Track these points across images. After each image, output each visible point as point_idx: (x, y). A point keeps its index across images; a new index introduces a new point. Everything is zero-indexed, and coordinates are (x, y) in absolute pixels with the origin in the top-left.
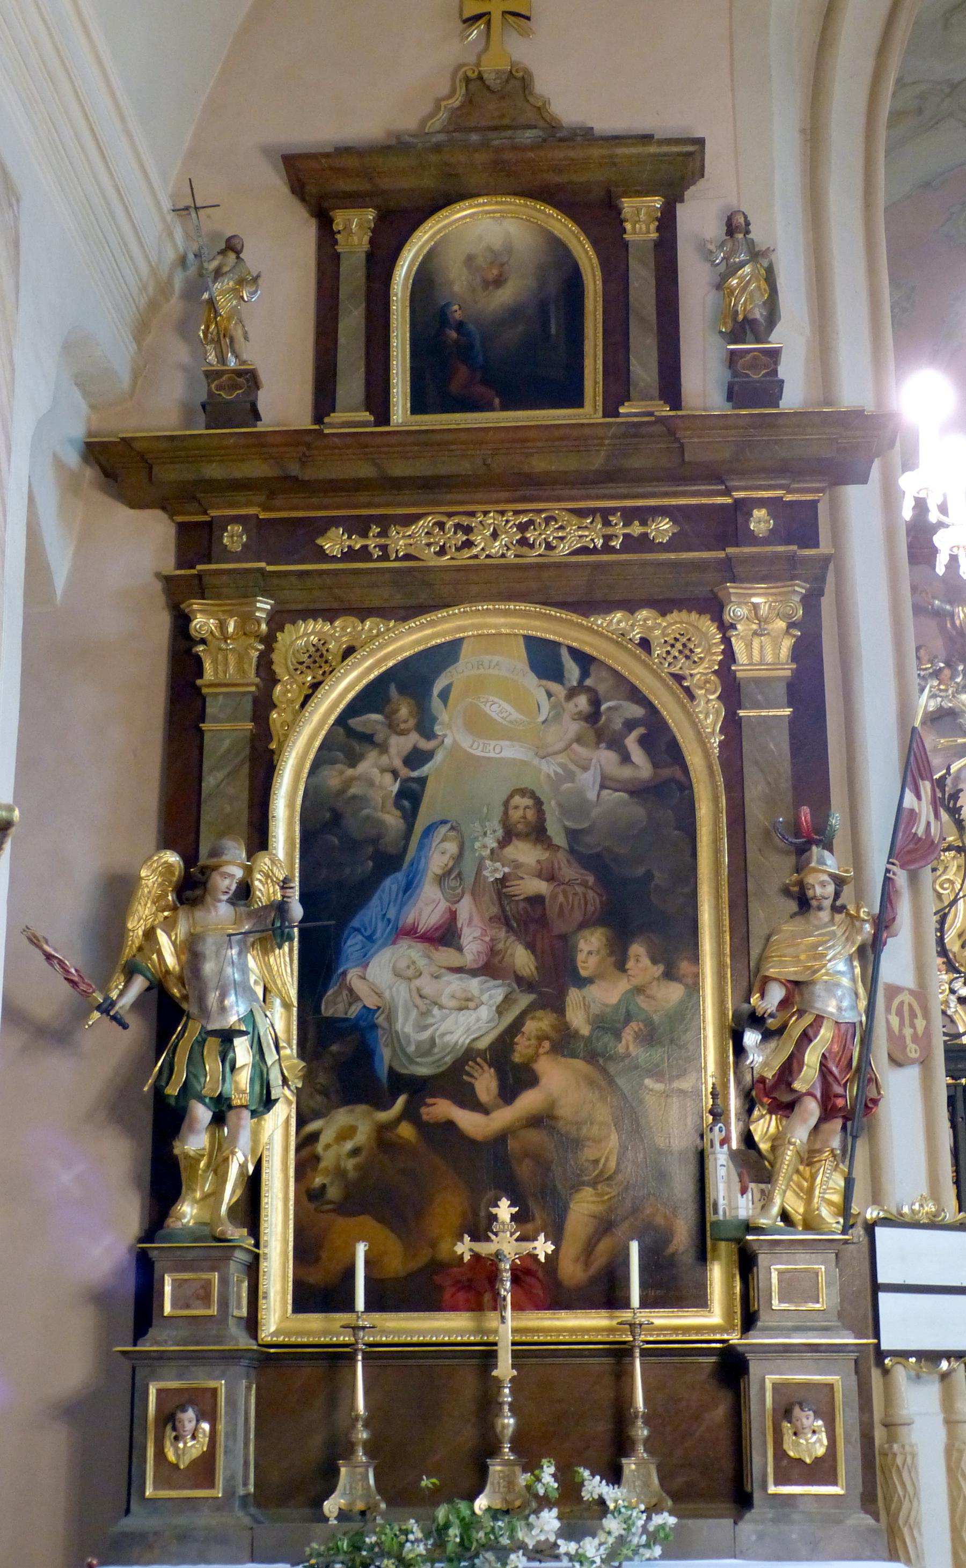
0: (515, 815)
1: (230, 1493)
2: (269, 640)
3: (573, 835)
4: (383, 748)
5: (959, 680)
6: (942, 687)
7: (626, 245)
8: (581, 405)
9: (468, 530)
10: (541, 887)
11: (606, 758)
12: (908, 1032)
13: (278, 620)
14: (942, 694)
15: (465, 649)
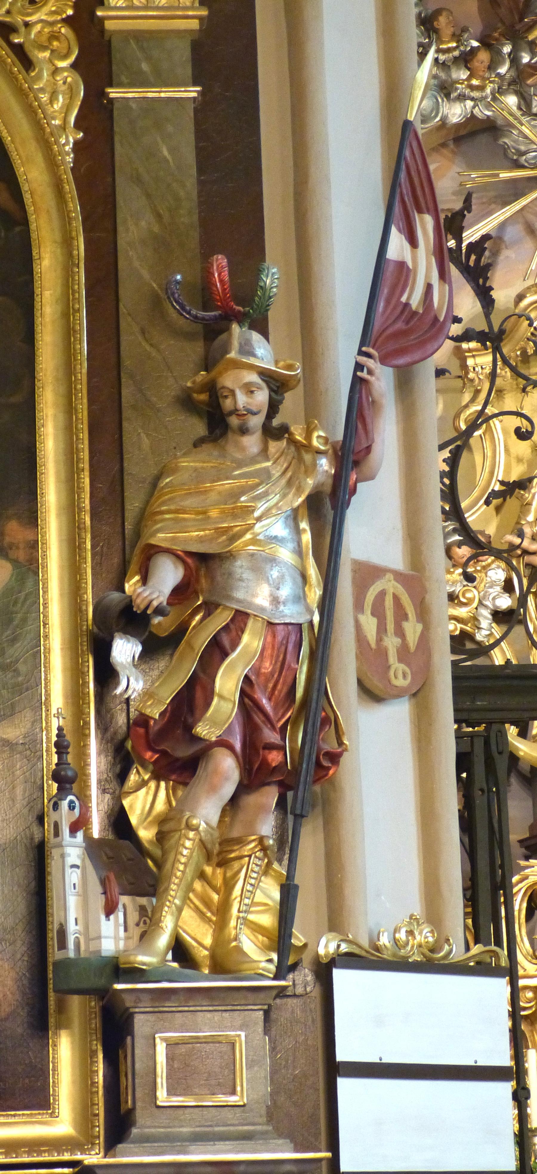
5: (503, 70)
6: (475, 82)
14: (475, 94)
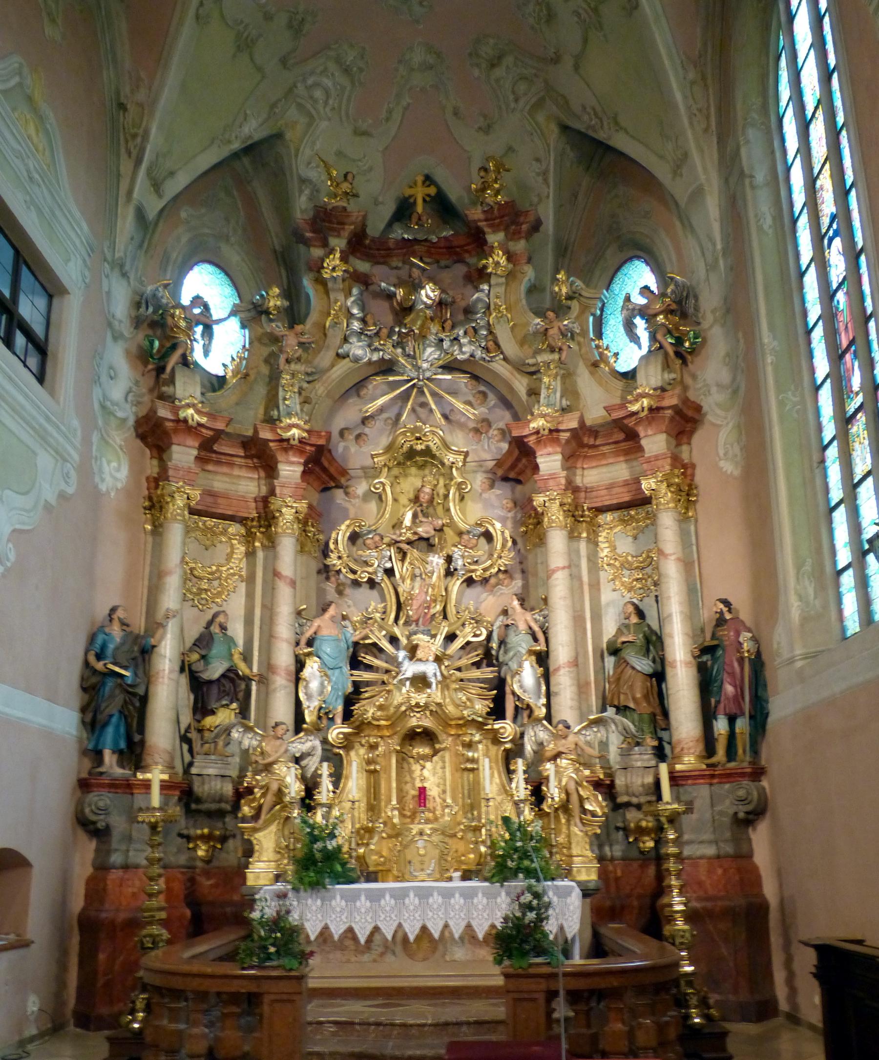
5: (395, 338)
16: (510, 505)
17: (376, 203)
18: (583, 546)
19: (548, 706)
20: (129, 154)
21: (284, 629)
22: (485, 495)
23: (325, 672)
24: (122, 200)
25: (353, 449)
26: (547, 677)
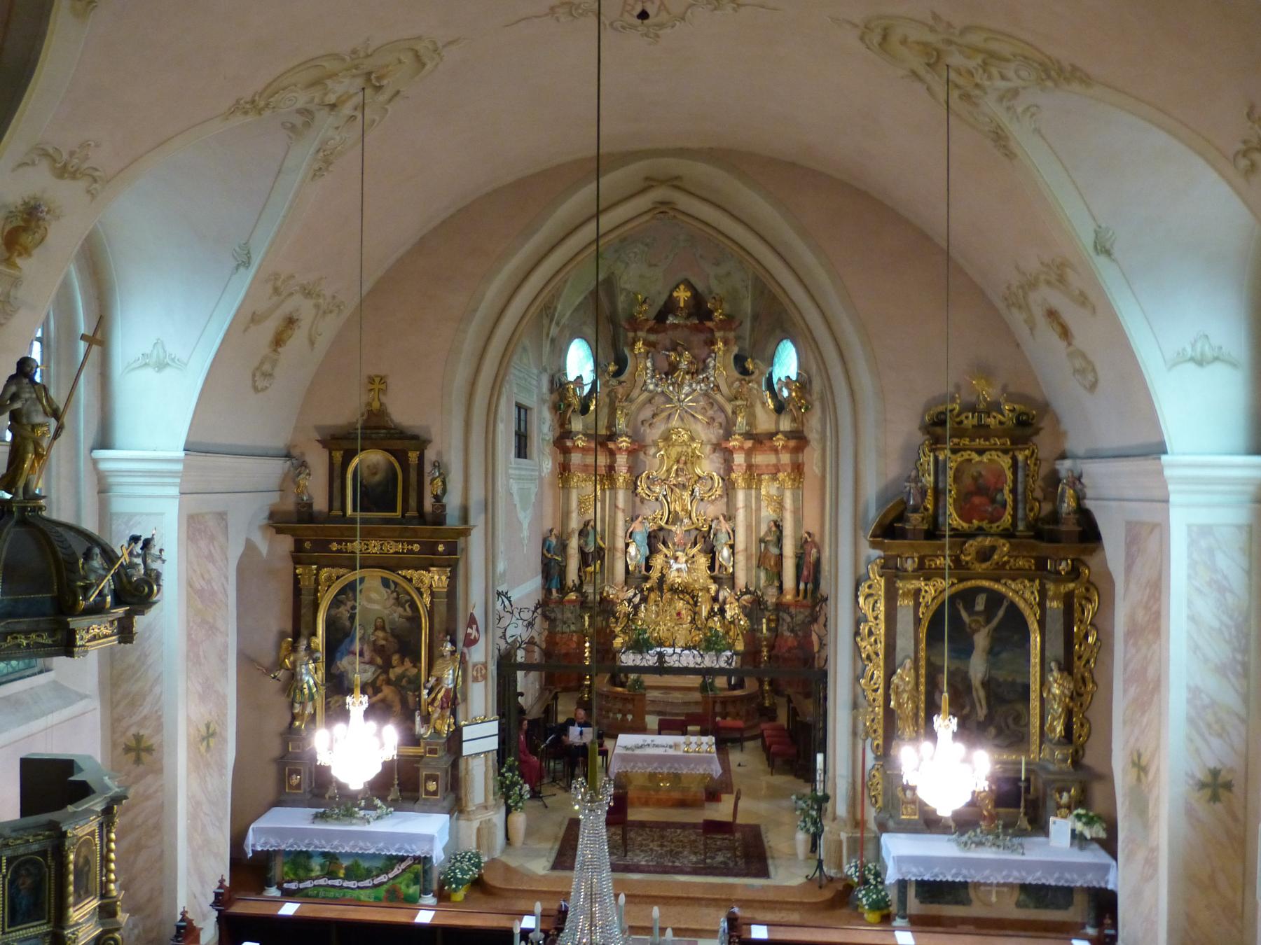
0: (378, 624)
1: (305, 792)
2: (317, 575)
3: (392, 630)
4: (345, 605)
7: (409, 465)
8: (396, 512)
9: (367, 545)
10: (383, 642)
11: (400, 610)
12: (479, 675)
13: (318, 570)
15: (366, 579)
16: (723, 461)
17: (659, 293)
18: (753, 492)
19: (733, 566)
20: (547, 316)
21: (620, 532)
22: (711, 456)
23: (638, 550)
24: (544, 337)
25: (648, 431)
26: (733, 554)
